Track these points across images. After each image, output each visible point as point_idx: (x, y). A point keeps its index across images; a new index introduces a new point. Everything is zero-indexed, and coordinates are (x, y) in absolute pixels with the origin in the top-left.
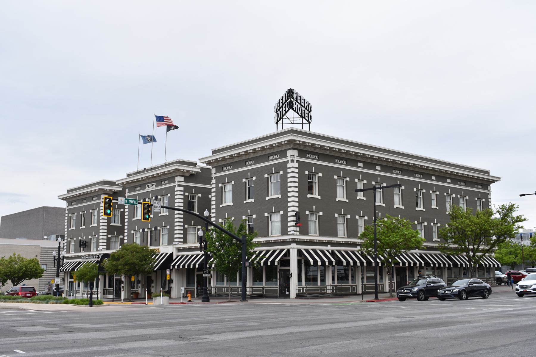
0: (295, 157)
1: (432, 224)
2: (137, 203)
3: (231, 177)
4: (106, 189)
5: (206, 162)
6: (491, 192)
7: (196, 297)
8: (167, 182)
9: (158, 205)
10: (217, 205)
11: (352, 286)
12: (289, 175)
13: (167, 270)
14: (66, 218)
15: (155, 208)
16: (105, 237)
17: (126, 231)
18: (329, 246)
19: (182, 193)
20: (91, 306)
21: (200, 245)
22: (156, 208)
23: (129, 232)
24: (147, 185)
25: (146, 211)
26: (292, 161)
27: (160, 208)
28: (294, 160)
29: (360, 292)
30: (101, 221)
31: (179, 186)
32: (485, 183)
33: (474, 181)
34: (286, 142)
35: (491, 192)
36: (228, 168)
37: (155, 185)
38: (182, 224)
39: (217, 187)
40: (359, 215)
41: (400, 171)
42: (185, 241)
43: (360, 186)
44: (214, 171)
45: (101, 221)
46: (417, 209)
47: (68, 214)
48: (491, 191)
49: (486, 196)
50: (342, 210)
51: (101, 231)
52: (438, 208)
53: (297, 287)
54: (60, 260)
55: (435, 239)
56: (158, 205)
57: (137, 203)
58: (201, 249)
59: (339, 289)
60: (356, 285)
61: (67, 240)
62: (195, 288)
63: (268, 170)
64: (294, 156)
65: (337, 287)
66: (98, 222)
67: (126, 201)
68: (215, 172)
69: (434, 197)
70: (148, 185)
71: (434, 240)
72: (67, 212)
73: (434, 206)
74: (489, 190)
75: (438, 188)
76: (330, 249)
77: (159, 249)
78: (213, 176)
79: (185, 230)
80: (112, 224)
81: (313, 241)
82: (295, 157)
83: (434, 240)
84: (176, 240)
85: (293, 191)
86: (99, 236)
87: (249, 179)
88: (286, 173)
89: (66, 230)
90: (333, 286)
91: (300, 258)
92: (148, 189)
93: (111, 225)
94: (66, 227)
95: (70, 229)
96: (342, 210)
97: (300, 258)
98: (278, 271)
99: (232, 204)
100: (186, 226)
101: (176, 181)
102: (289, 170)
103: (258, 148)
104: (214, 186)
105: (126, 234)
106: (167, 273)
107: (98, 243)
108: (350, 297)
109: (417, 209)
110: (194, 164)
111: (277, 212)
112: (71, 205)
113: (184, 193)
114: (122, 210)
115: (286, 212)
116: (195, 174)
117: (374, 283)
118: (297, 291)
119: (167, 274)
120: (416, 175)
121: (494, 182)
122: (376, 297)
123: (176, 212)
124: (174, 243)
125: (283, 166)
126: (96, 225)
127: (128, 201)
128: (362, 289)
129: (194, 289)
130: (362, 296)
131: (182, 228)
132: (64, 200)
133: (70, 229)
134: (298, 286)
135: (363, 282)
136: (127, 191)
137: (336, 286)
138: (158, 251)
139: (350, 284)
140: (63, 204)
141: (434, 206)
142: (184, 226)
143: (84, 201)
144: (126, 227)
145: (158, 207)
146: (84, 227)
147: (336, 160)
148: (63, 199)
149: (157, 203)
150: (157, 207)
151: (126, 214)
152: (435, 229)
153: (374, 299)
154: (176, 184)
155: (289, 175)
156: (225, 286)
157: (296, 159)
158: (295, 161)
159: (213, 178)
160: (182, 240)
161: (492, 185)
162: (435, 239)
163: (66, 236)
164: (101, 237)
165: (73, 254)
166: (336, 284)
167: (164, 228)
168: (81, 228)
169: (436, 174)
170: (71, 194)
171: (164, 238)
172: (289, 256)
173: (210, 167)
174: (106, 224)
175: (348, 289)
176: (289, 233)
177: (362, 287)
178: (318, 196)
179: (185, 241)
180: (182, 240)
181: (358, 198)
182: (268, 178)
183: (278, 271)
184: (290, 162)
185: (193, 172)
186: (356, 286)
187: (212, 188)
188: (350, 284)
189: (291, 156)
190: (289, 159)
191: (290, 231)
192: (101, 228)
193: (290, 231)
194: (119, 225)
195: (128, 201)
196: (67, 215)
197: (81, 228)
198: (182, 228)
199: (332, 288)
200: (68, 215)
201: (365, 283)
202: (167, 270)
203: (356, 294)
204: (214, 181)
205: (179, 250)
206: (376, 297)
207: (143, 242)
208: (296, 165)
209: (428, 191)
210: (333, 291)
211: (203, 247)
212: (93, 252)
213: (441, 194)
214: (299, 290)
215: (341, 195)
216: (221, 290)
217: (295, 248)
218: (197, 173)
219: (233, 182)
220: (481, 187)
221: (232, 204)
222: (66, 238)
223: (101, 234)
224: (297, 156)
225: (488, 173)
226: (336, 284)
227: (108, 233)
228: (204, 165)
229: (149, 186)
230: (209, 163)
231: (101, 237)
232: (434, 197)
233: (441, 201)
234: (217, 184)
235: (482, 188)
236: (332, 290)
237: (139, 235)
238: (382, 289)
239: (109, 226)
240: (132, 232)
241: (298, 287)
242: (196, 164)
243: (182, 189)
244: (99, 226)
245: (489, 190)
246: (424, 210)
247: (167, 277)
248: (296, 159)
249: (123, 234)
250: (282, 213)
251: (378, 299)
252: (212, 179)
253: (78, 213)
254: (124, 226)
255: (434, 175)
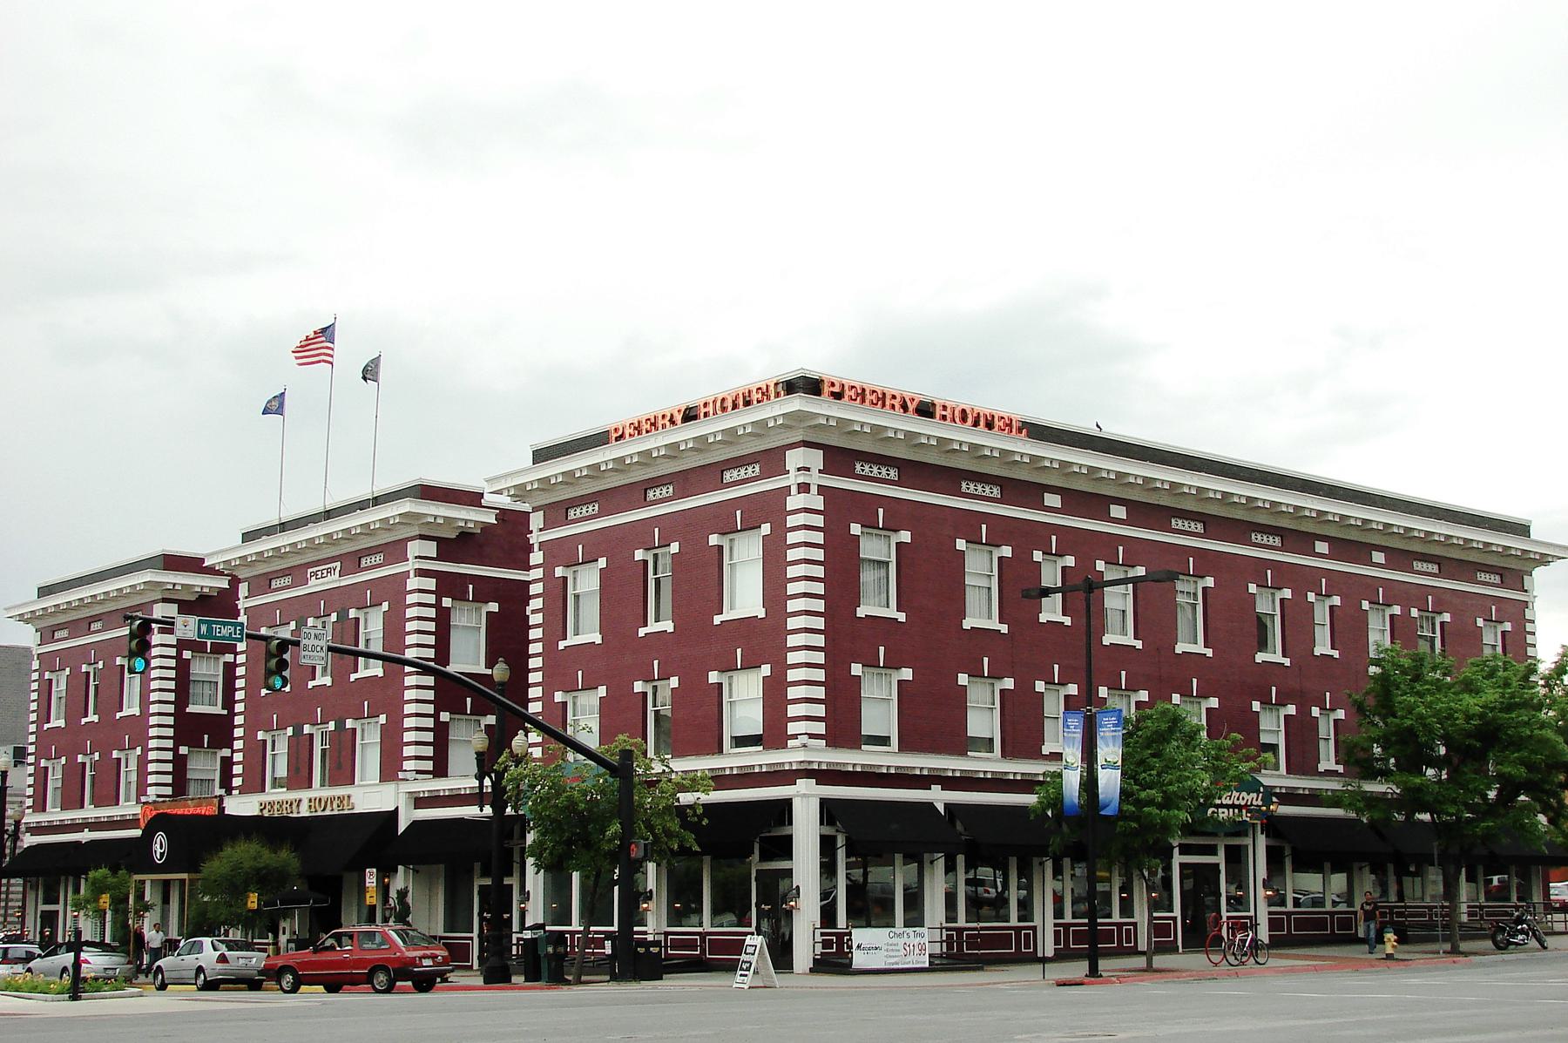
0: (814, 471)
1: (1315, 711)
2: (241, 634)
3: (596, 545)
4: (198, 586)
5: (508, 489)
6: (1535, 597)
7: (476, 966)
8: (379, 558)
9: (316, 642)
10: (549, 642)
11: (1018, 930)
12: (792, 538)
13: (368, 870)
14: (35, 686)
15: (306, 653)
16: (169, 755)
17: (238, 732)
18: (936, 788)
19: (431, 599)
20: (75, 997)
21: (477, 783)
22: (311, 653)
23: (249, 737)
24: (309, 571)
25: (274, 661)
26: (804, 488)
27: (323, 655)
28: (809, 484)
29: (1050, 953)
30: (154, 697)
31: (421, 573)
32: (1513, 565)
33: (1473, 557)
34: (780, 421)
35: (1535, 597)
36: (578, 511)
37: (338, 568)
38: (430, 709)
39: (548, 578)
40: (1047, 681)
41: (1200, 522)
42: (440, 770)
43: (1051, 575)
44: (536, 521)
45: (154, 697)
46: (1260, 657)
47: (41, 672)
48: (1535, 594)
49: (1519, 614)
50: (986, 660)
51: (153, 732)
52: (1336, 654)
53: (818, 932)
54: (6, 836)
55: (1328, 762)
56: (316, 642)
57: (241, 634)
58: (478, 798)
59: (973, 941)
60: (1136, 923)
61: (36, 764)
62: (475, 934)
63: (724, 519)
64: (808, 469)
65: (576, 936)
66: (145, 702)
67: (204, 628)
68: (542, 526)
69: (1322, 615)
70: (315, 569)
71: (1321, 768)
72: (36, 665)
73: (1323, 647)
74: (1526, 591)
75: (1338, 583)
76: (938, 800)
77: (349, 797)
78: (534, 539)
79: (441, 731)
80: (191, 709)
81: (877, 771)
82: (814, 471)
83: (1321, 768)
84: (408, 765)
85: (806, 595)
86: (146, 750)
87: (656, 551)
88: (780, 530)
89: (33, 728)
90: (948, 929)
91: (828, 831)
92: (314, 585)
93: (188, 710)
94: (33, 717)
95: (46, 726)
96: (986, 660)
97: (828, 831)
98: (754, 875)
99: (598, 639)
100: (445, 716)
101: (410, 555)
102: (792, 521)
103: (686, 442)
104: (537, 573)
105: (238, 745)
106: (368, 880)
107: (142, 773)
108: (1011, 968)
109: (1260, 657)
110: (473, 499)
111: (751, 665)
112: (53, 640)
113: (439, 600)
114: (229, 658)
115: (781, 667)
116: (479, 531)
117: (1086, 921)
118: (819, 949)
119: (367, 885)
120: (1259, 536)
121: (1544, 560)
122: (1094, 971)
123: (408, 669)
124: (401, 775)
125: (769, 509)
126: (136, 711)
127: (210, 629)
128: (1057, 942)
129: (471, 939)
130: (1042, 966)
131: (430, 723)
132: (27, 621)
133: (46, 726)
134: (821, 928)
135: (1059, 913)
136: (243, 589)
137: (960, 931)
138: (345, 802)
139: (1014, 922)
140: (27, 637)
141: (1323, 647)
142: (436, 716)
143: (96, 626)
144: (239, 720)
145: (319, 649)
146: (95, 718)
147: (964, 485)
148: (21, 618)
149: (313, 636)
150: (314, 648)
151: (240, 671)
152: (1326, 729)
153: (1086, 976)
154: (411, 565)
155: (792, 538)
156: (707, 927)
157: (816, 479)
158: (814, 489)
159: (536, 547)
160: (429, 765)
161: (1538, 572)
162: (1328, 762)
163: (31, 749)
164: (152, 755)
165: (55, 814)
166: (961, 922)
167: (366, 721)
168: (84, 721)
169: (1332, 532)
170: (50, 602)
171: (369, 759)
172: (791, 823)
173: (526, 507)
174: (171, 709)
175: (1003, 941)
176: (791, 743)
177: (1057, 933)
178: (1063, 615)
179: (440, 770)
180: (429, 765)
181: (1043, 618)
182: (720, 548)
183: (754, 875)
184: (794, 490)
185: (471, 525)
186: (1034, 929)
187: (530, 582)
188: (1116, 918)
189: (799, 469)
190: (792, 479)
191: (795, 737)
192: (153, 720)
193: (795, 737)
194: (218, 710)
195: (210, 629)
196: (35, 676)
197: (84, 721)
198: (430, 723)
199: (944, 938)
200: (41, 675)
201: (1068, 919)
202: (368, 870)
203: (1033, 959)
204: (536, 557)
205: (420, 802)
206: (1094, 971)
207: (298, 770)
208: (818, 502)
209: (1299, 593)
210: (950, 947)
211: (490, 790)
212: (128, 808)
213: (1352, 602)
214: (826, 944)
215: (981, 614)
216: (691, 945)
217: (813, 796)
218: (486, 527)
219: (602, 562)
220: (1498, 577)
221: (598, 639)
222: (31, 759)
223: (153, 744)
224: (820, 471)
225: (1522, 530)
226: (961, 922)
227: (178, 740)
228: (504, 501)
229: (319, 573)
230: (521, 492)
231: (152, 755)
232: (1322, 615)
233: (1348, 628)
234: (548, 566)
235: (1502, 585)
236: (944, 944)
237: (282, 748)
238: (1129, 941)
239: (180, 714)
240: (260, 735)
241: (822, 934)
242: (481, 495)
243: (431, 583)
244: (145, 714)
245: (1526, 591)
246: (1287, 662)
247: (368, 895)
248: (816, 479)
249: (228, 742)
250: (766, 670)
251: (1101, 976)
252: (530, 549)
253: (75, 672)
254: (232, 714)
255: (1323, 538)
